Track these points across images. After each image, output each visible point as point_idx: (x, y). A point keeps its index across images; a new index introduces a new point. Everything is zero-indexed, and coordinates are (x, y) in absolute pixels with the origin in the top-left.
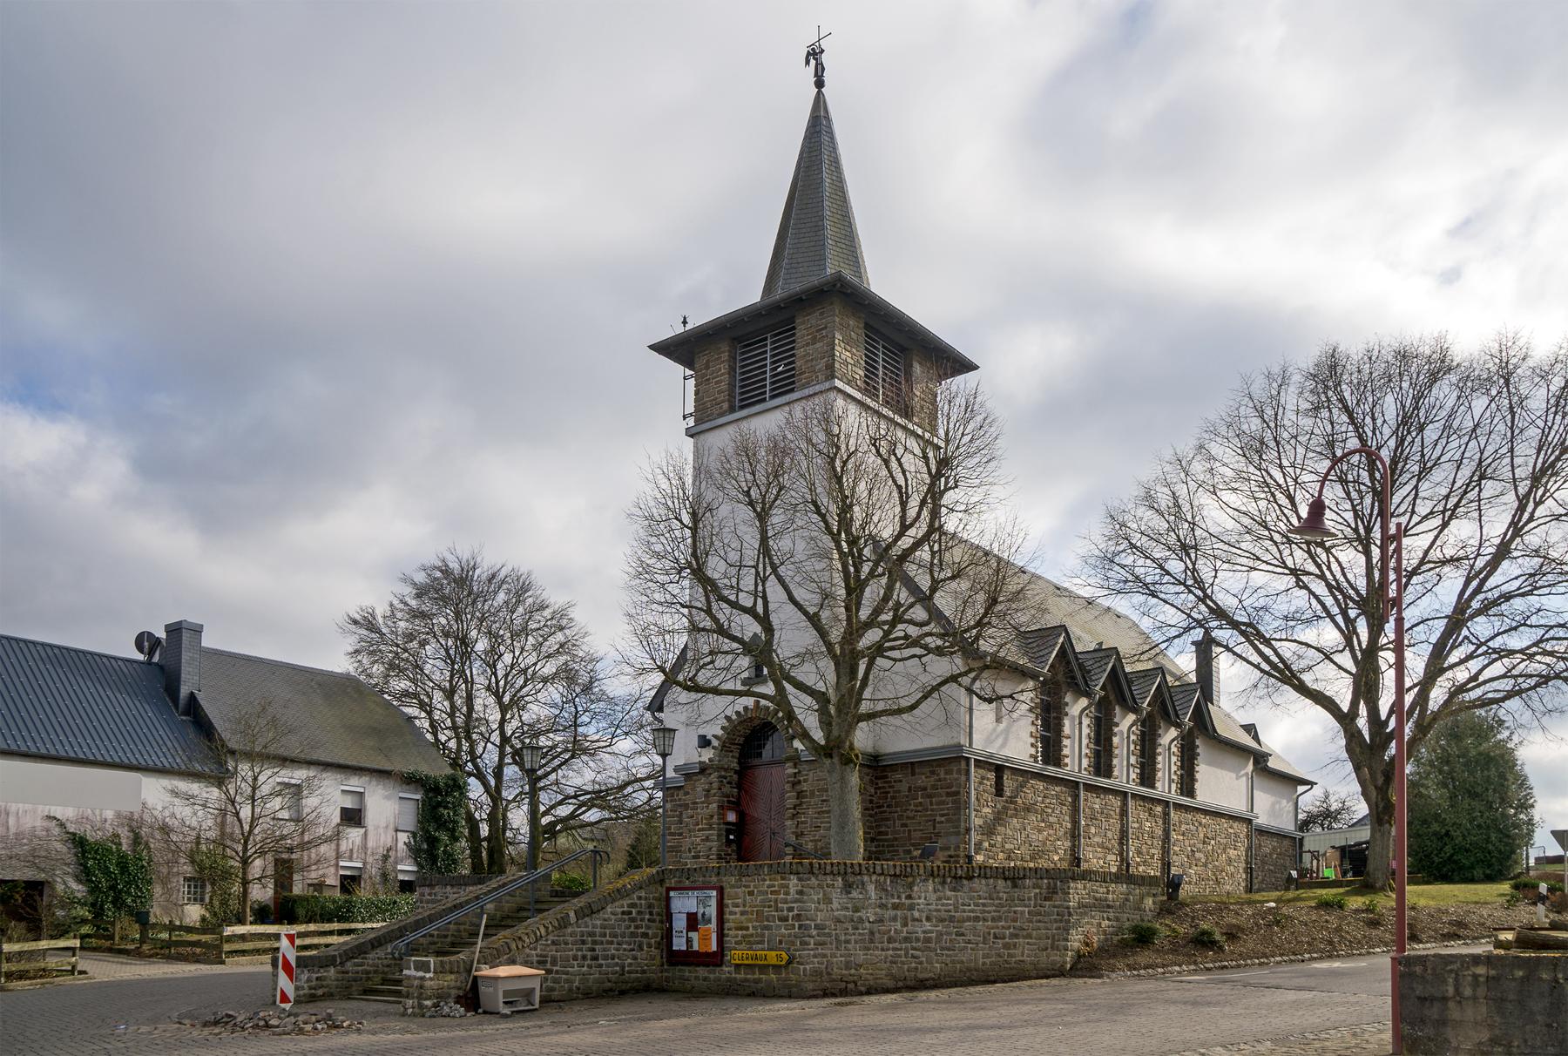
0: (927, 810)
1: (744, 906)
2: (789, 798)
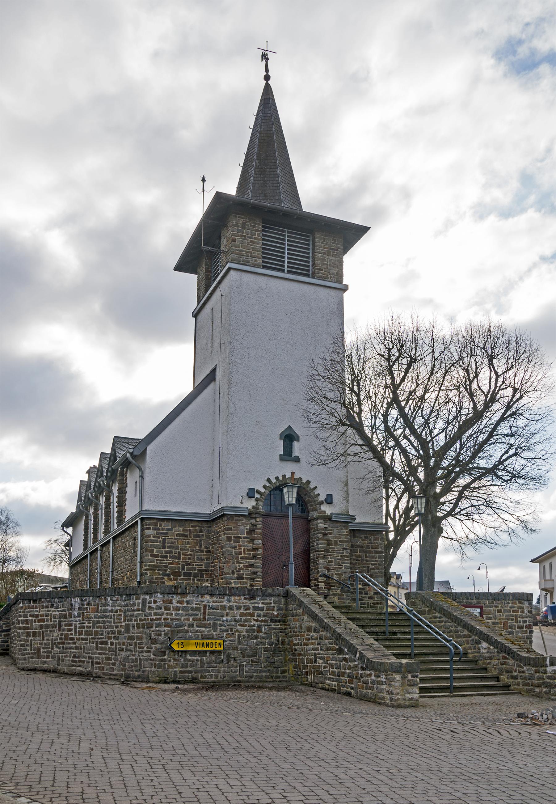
0: (363, 560)
1: (495, 619)
2: (321, 544)
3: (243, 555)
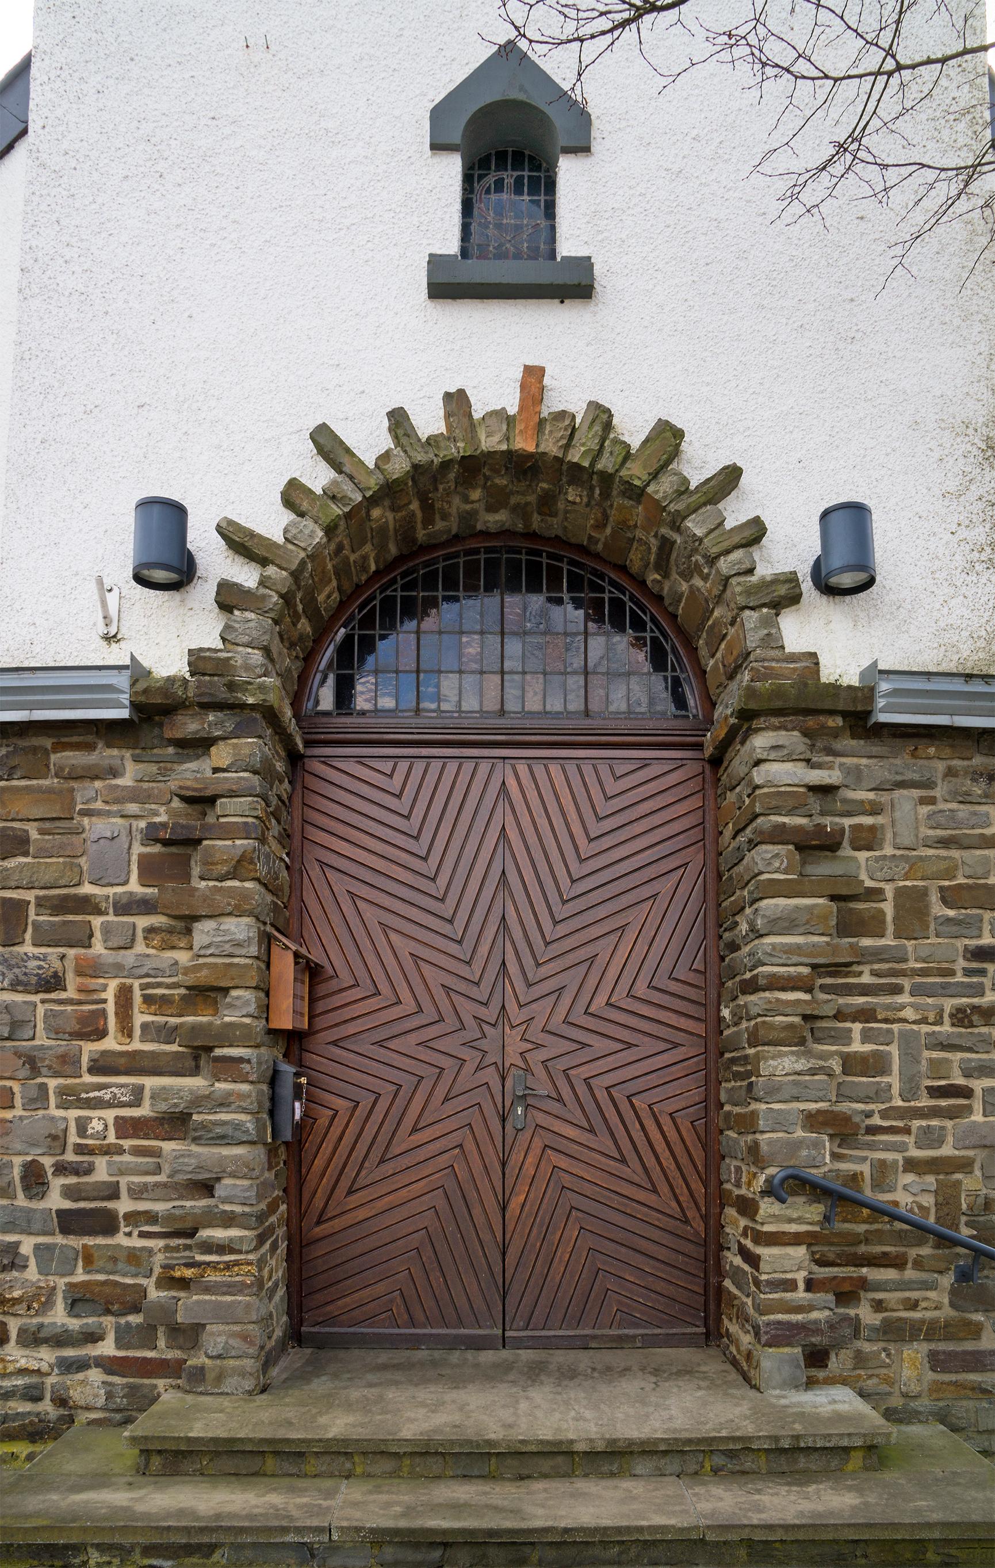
3: (111, 1043)
